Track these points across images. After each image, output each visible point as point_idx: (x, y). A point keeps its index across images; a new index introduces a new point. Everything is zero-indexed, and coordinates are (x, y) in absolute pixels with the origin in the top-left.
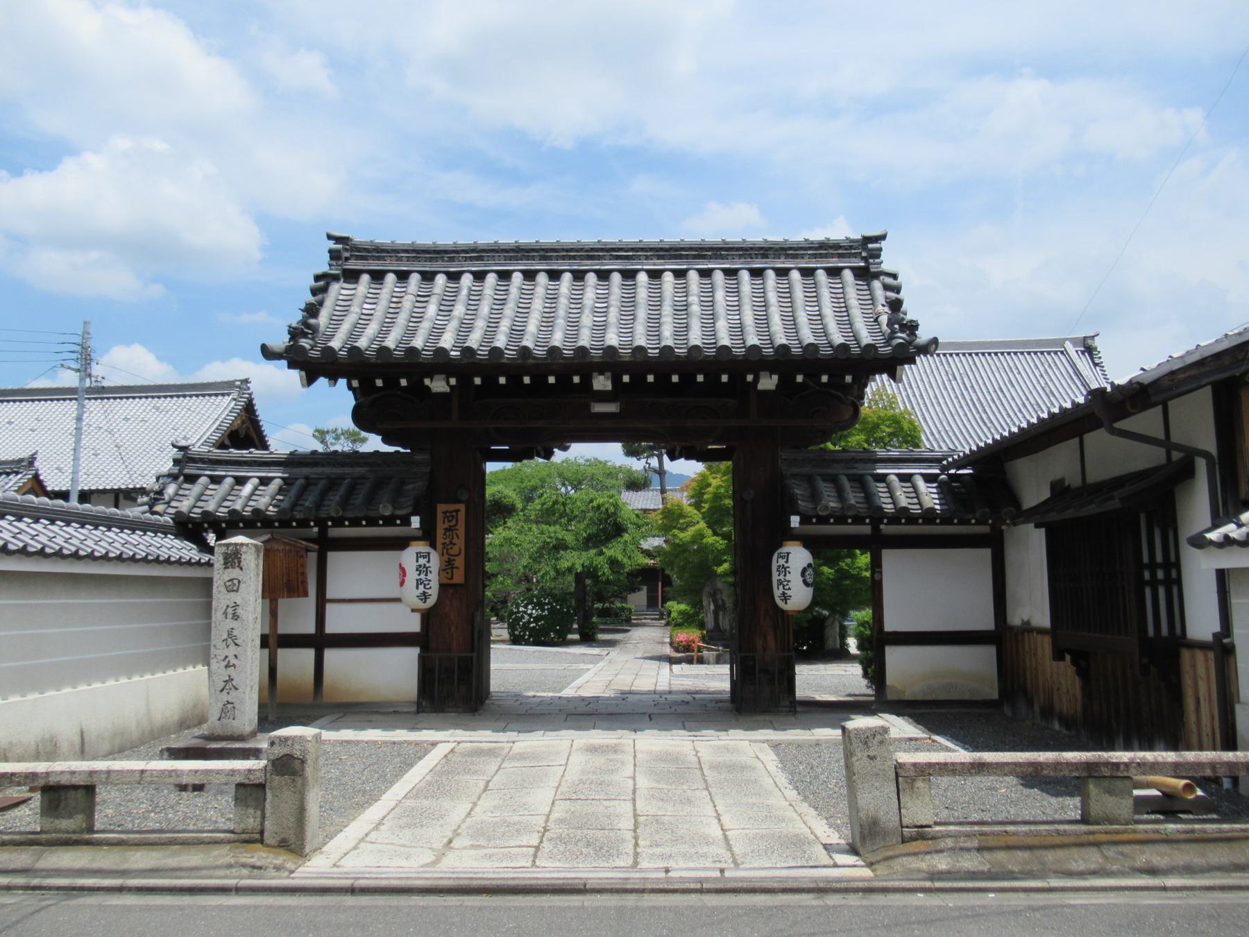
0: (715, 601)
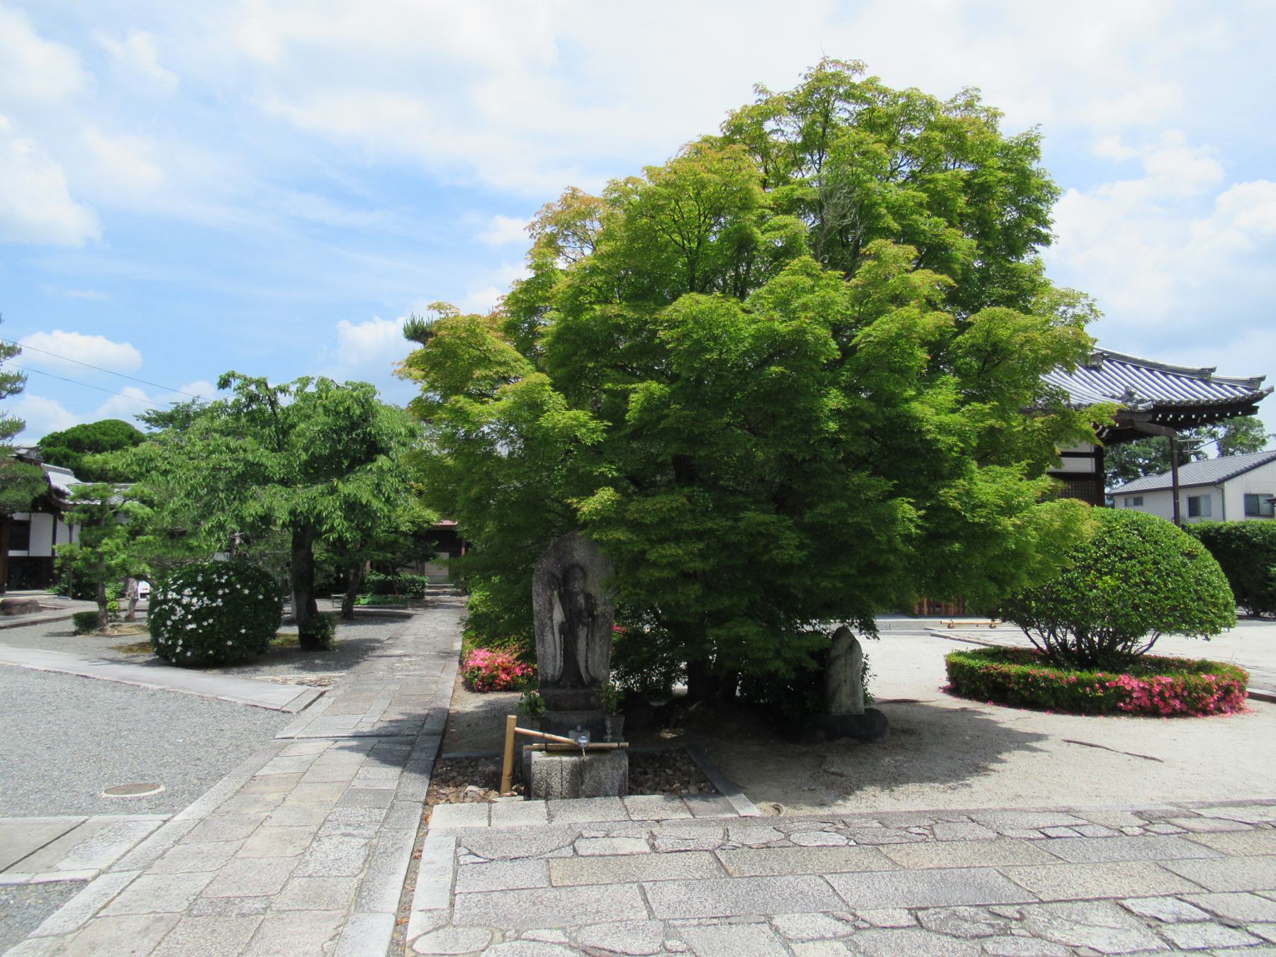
0: (567, 598)
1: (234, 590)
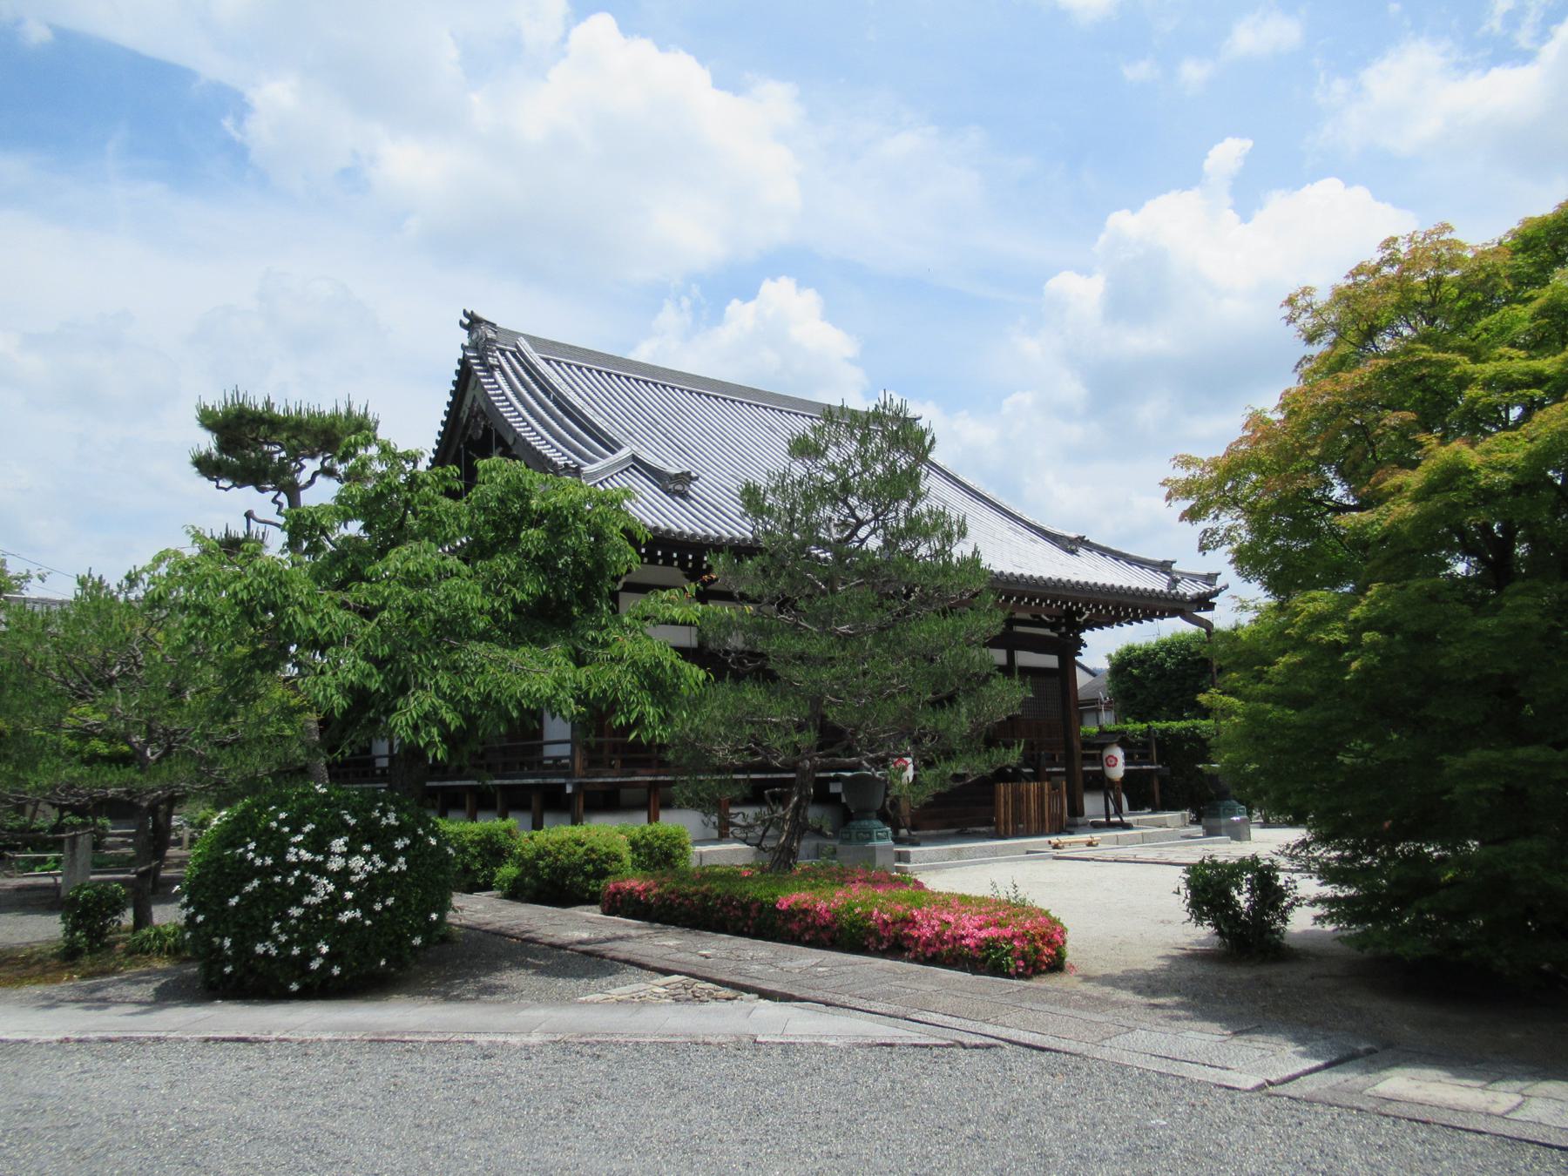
1: (416, 839)
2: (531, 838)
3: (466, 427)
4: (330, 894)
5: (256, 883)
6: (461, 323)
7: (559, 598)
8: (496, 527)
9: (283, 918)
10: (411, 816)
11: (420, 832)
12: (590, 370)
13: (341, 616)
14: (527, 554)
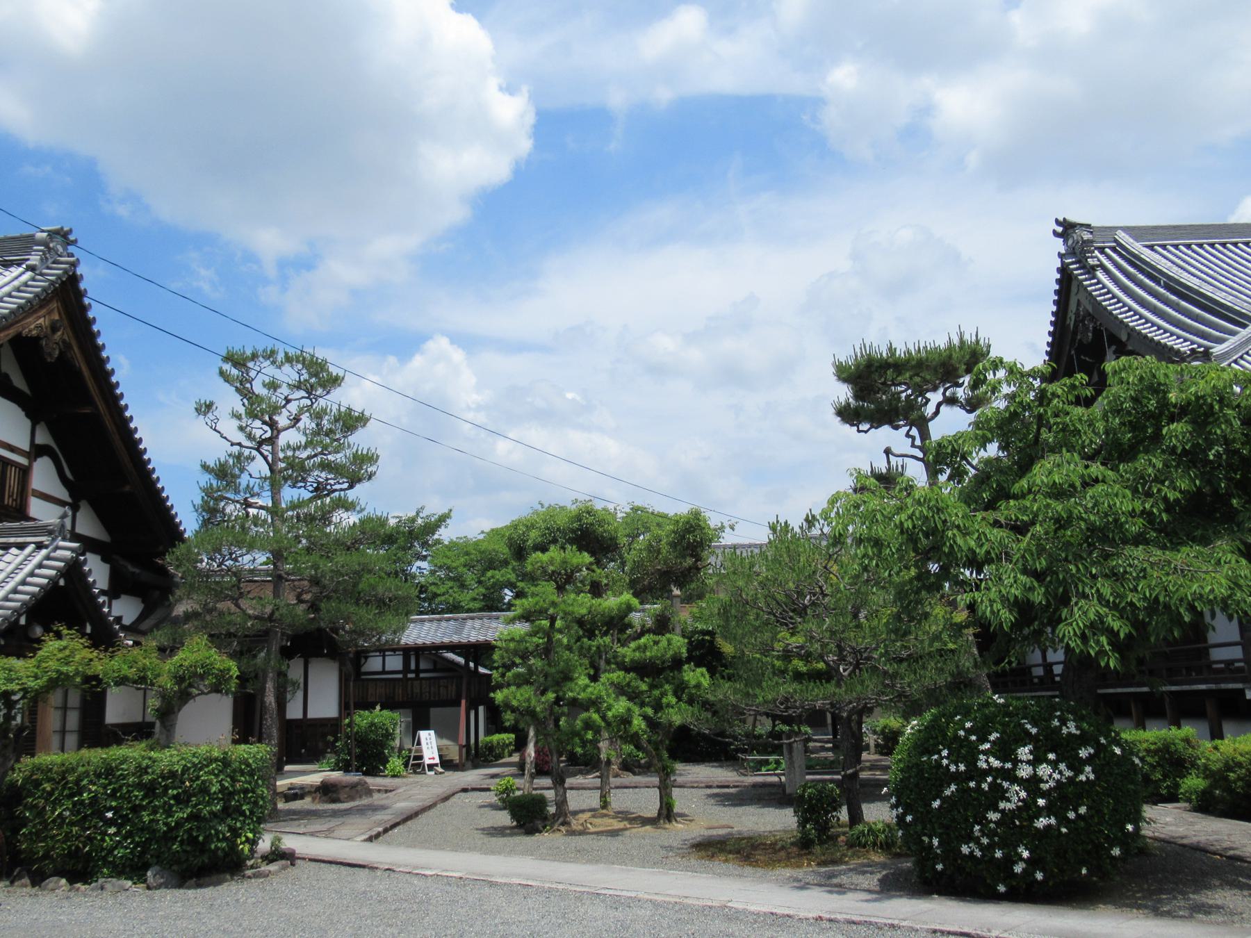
1: (1099, 748)
2: (1216, 748)
3: (1075, 332)
4: (1023, 800)
5: (953, 787)
6: (1055, 233)
7: (1215, 491)
8: (1134, 427)
9: (983, 821)
10: (1090, 725)
11: (1103, 741)
12: (1200, 246)
13: (996, 534)
14: (1173, 450)
